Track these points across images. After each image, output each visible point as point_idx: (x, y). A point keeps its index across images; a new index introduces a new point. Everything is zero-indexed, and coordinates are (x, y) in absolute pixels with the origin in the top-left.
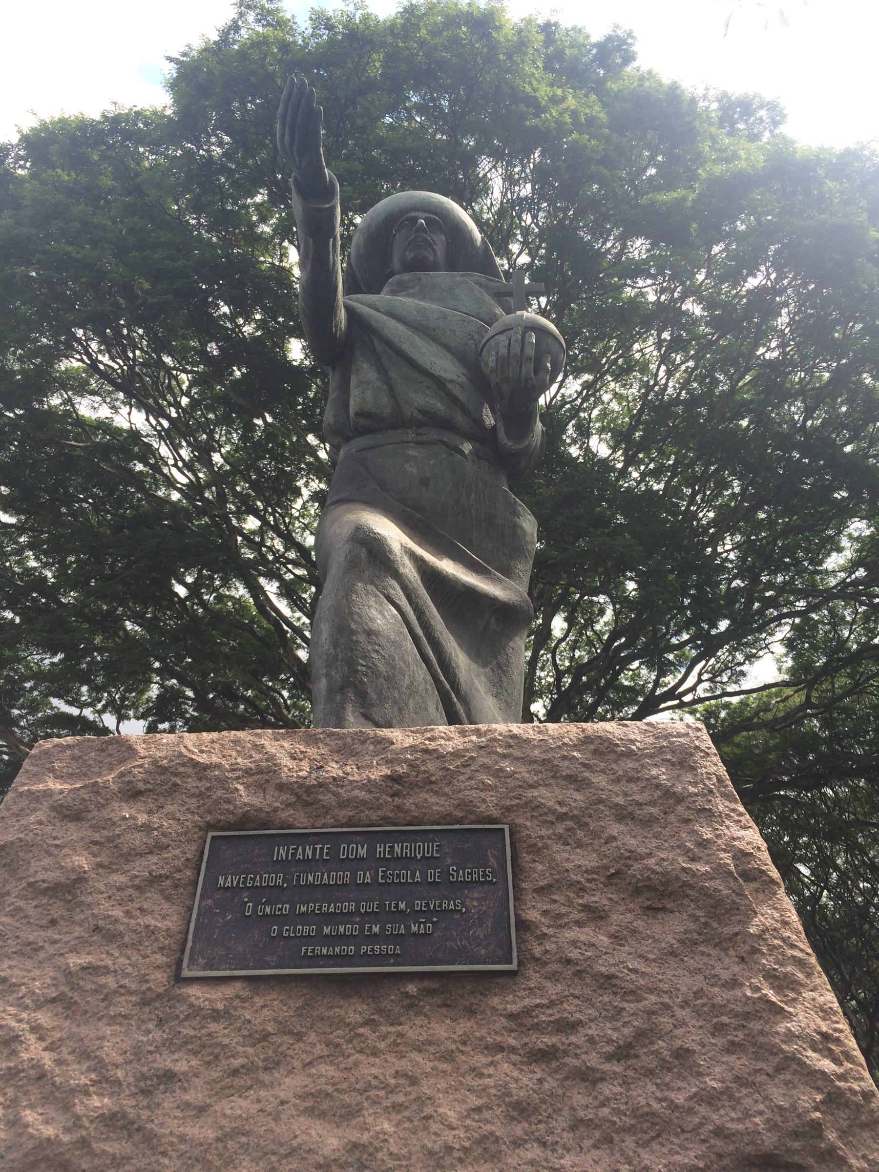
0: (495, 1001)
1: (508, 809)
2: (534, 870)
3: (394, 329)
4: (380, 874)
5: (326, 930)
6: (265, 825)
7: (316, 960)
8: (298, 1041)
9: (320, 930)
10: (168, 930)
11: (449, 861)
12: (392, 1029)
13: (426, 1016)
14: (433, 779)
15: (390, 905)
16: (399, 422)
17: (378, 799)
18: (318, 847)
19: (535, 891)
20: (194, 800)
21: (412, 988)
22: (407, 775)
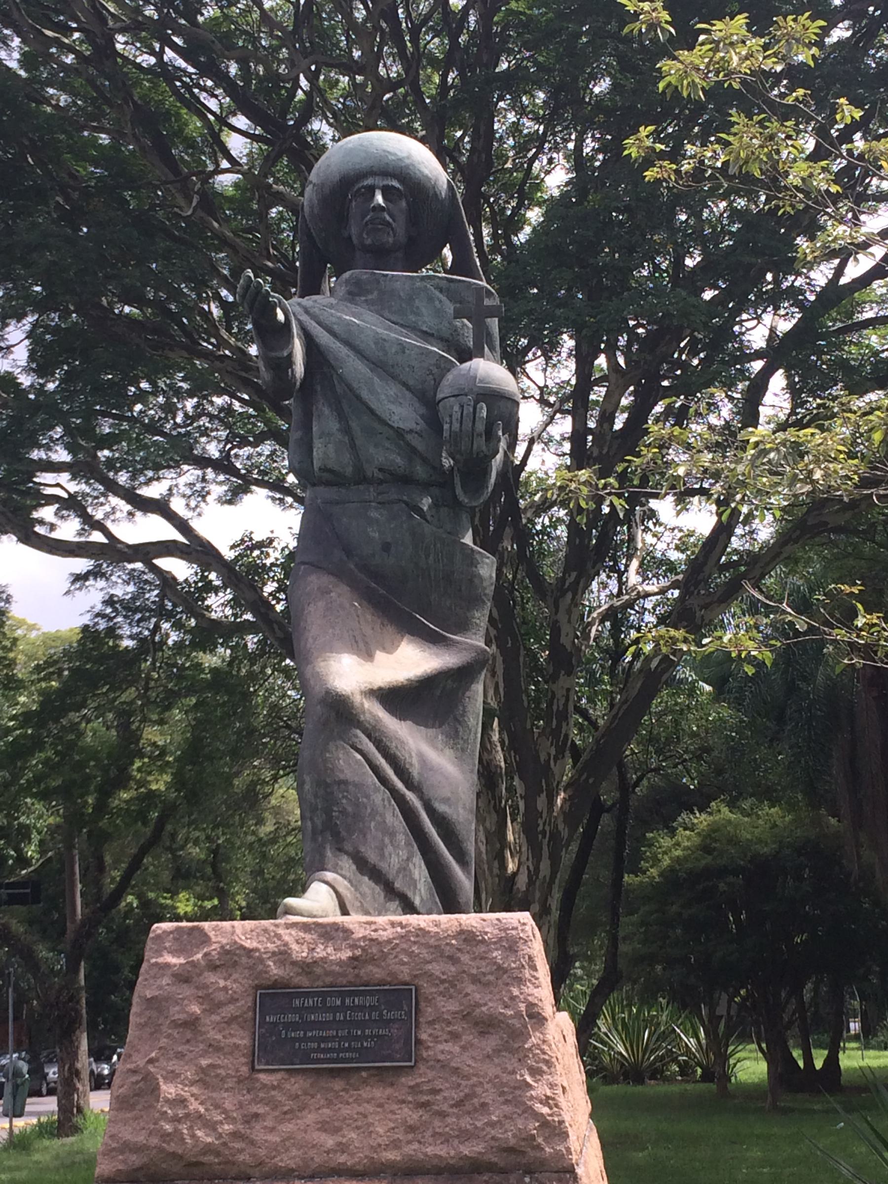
3: (353, 367)
16: (361, 478)
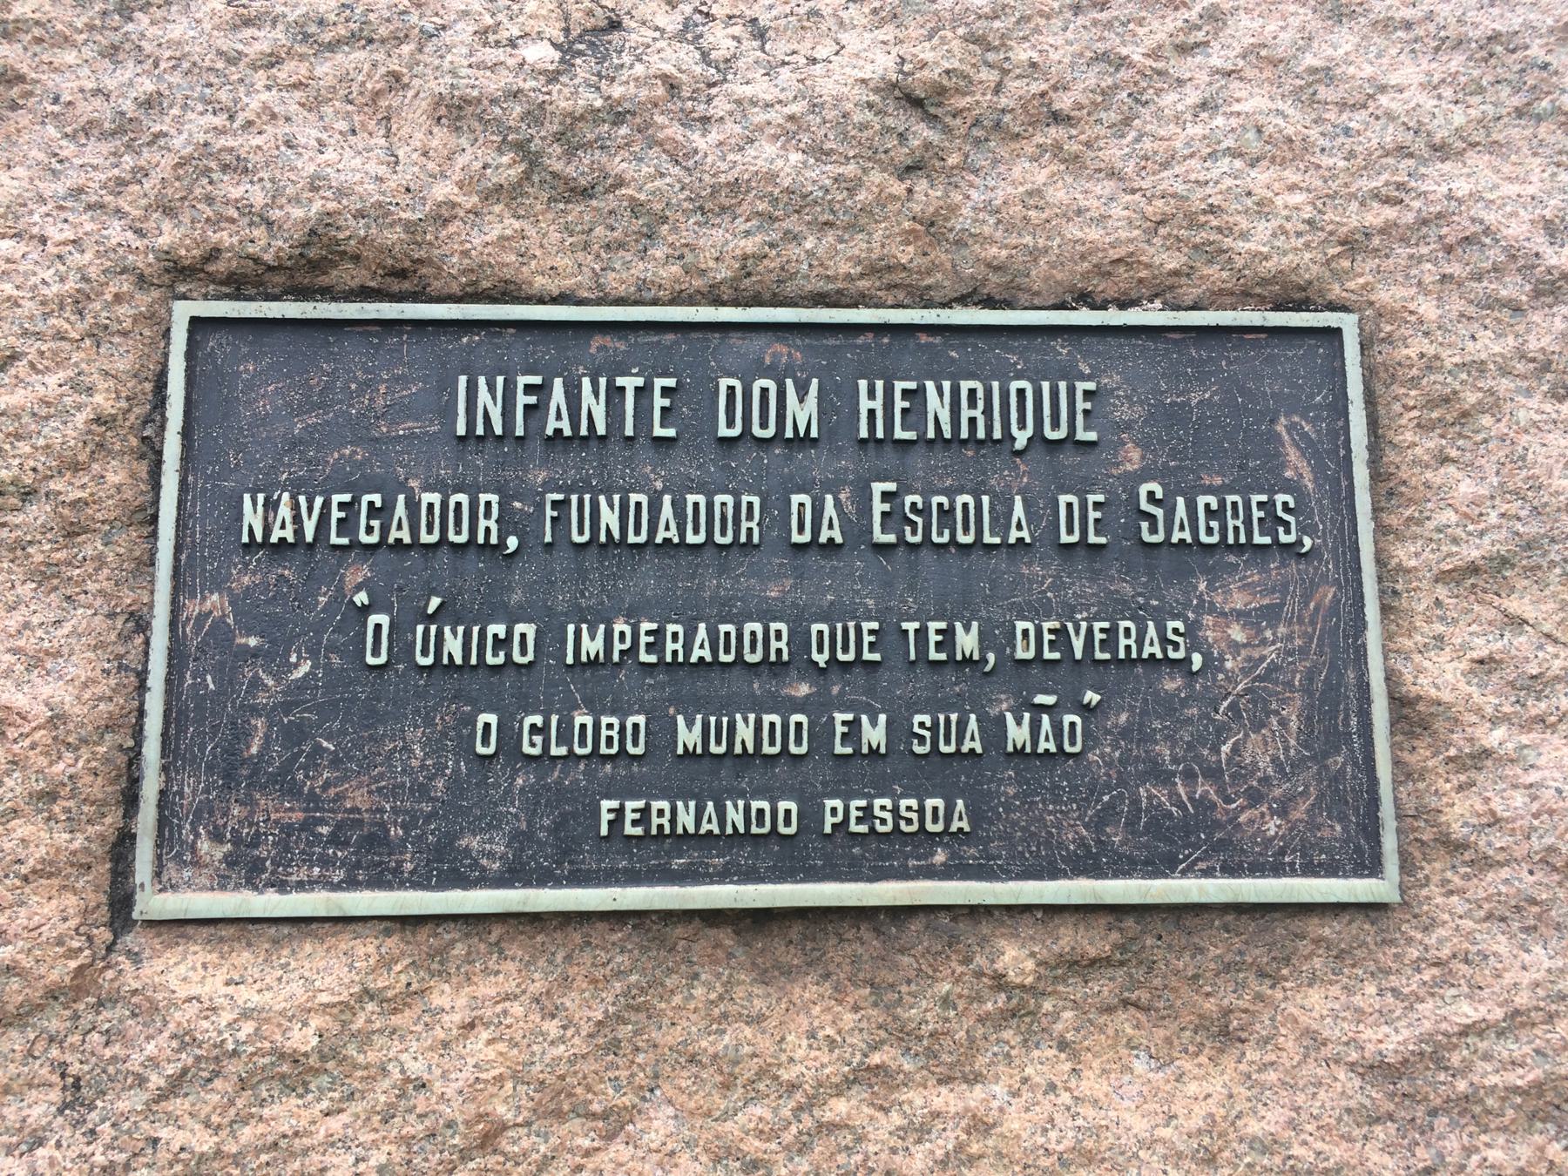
0: (1315, 1003)
1: (1352, 244)
2: (1439, 492)
4: (879, 507)
5: (688, 736)
6: (403, 278)
7: (658, 854)
8: (610, 1137)
9: (661, 732)
10: (57, 719)
11: (1133, 458)
12: (945, 1099)
13: (1063, 1045)
14: (1063, 102)
15: (922, 633)
17: (852, 186)
18: (630, 383)
19: (1442, 577)
20: (96, 152)
21: (1014, 958)
22: (961, 81)
